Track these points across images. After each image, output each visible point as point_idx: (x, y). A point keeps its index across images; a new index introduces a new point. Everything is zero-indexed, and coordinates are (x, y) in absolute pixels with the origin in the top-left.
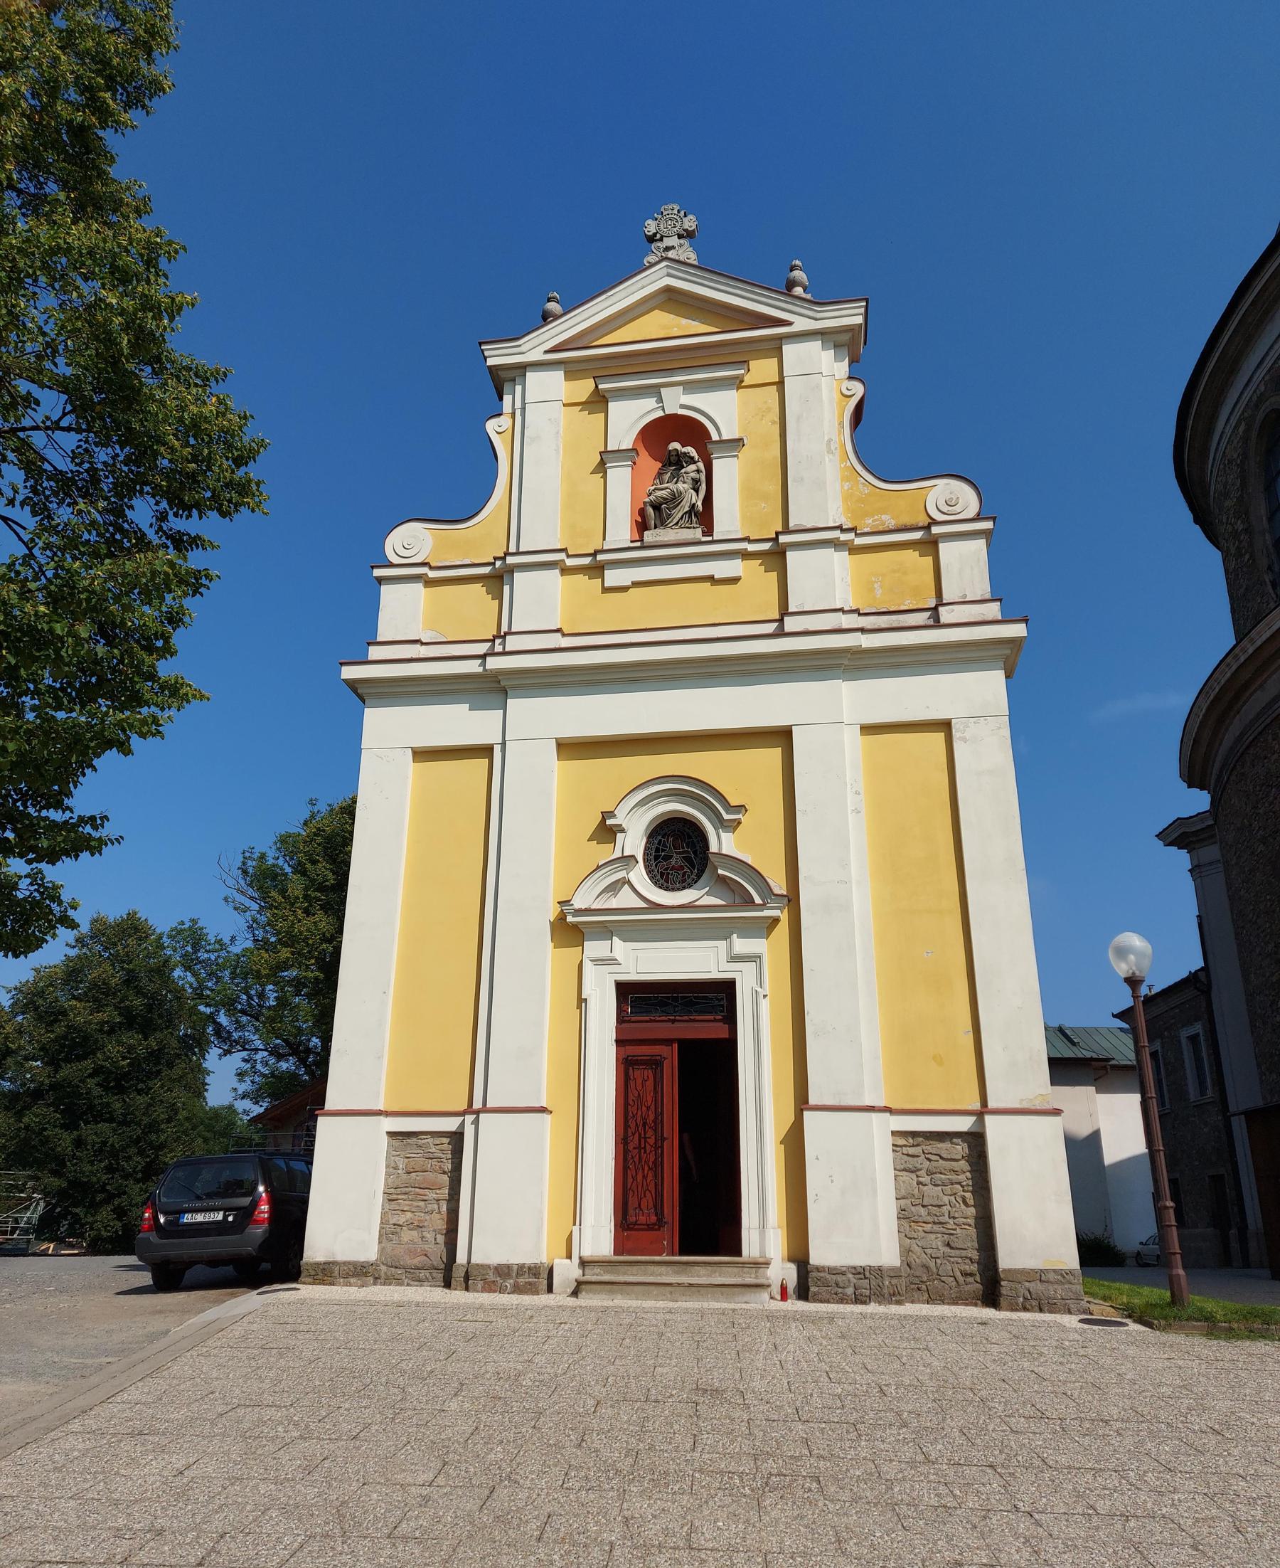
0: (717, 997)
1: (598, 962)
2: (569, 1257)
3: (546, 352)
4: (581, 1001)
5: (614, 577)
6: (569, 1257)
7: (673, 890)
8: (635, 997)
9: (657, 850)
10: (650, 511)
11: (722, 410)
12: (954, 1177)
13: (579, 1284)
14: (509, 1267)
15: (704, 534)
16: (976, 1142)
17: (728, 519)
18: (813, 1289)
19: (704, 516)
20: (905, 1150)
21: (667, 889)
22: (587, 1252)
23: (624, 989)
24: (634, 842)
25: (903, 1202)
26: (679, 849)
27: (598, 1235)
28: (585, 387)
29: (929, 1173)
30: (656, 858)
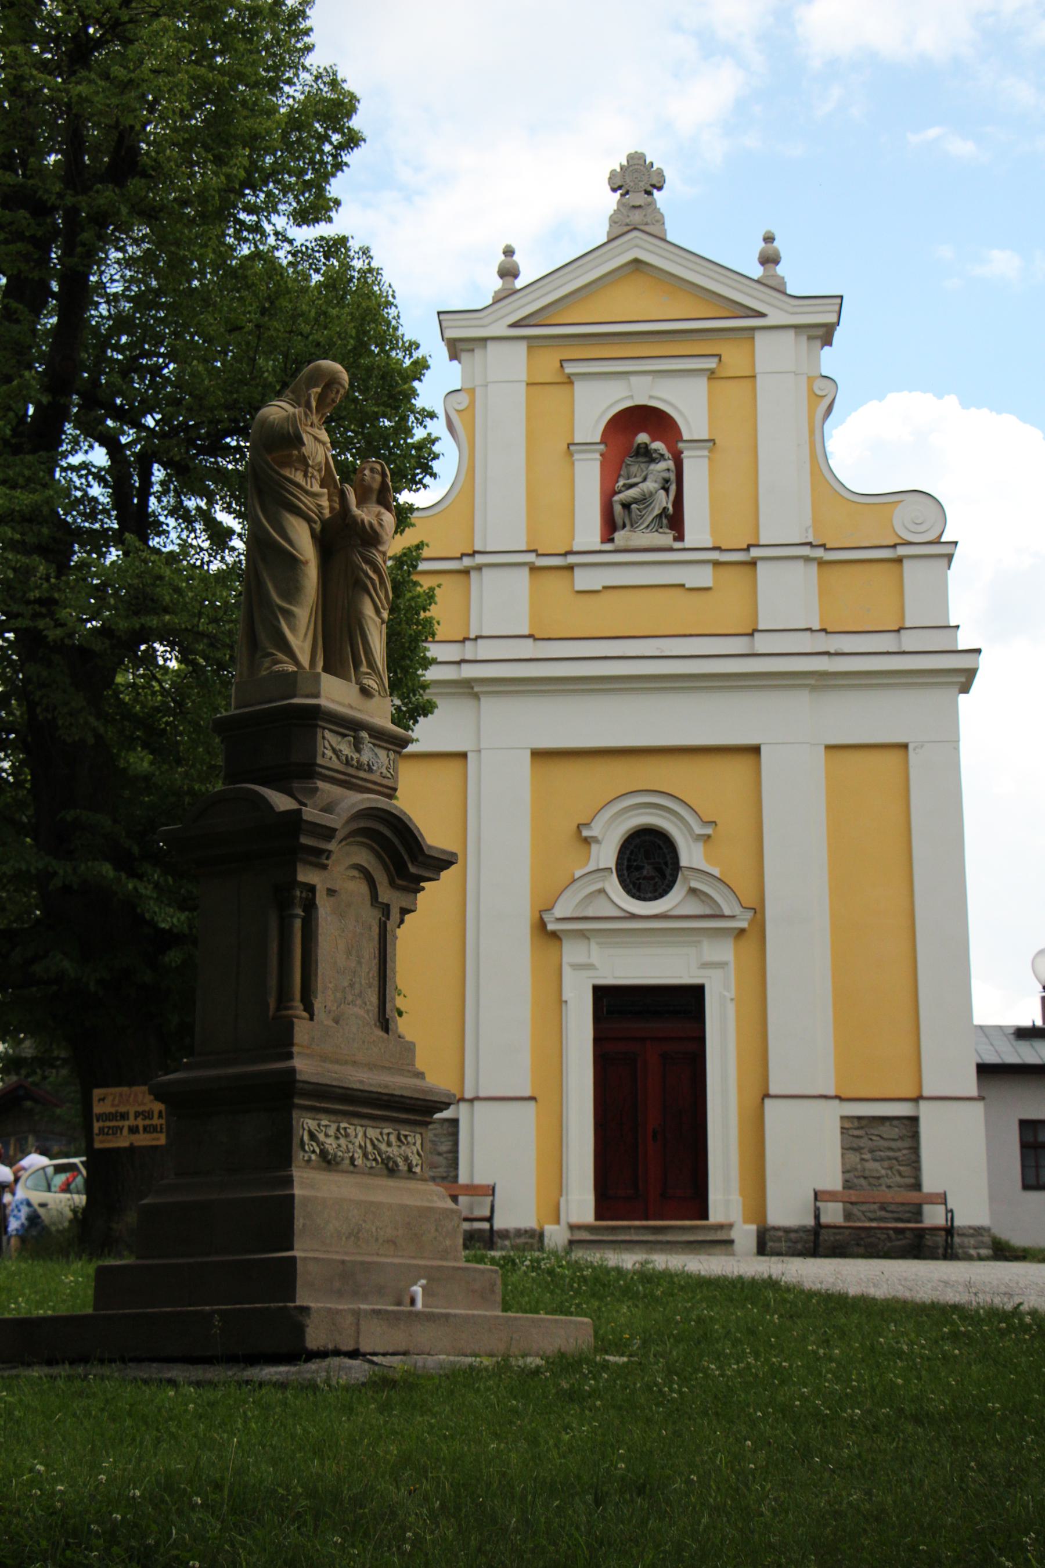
0: (686, 1003)
1: (577, 967)
2: (558, 1222)
3: (514, 325)
4: (561, 1002)
5: (584, 580)
6: (558, 1222)
7: (645, 900)
8: (611, 1002)
9: (629, 860)
10: (618, 509)
11: (687, 403)
12: (891, 1154)
13: (571, 1242)
14: (507, 1231)
15: (676, 539)
16: (914, 1120)
17: (698, 528)
18: (770, 1244)
19: (674, 520)
20: (851, 1132)
21: (639, 898)
22: (575, 1220)
23: (601, 993)
24: (607, 854)
25: (848, 1176)
26: (648, 862)
27: (580, 1203)
28: (549, 362)
29: (871, 1151)
30: (629, 868)
